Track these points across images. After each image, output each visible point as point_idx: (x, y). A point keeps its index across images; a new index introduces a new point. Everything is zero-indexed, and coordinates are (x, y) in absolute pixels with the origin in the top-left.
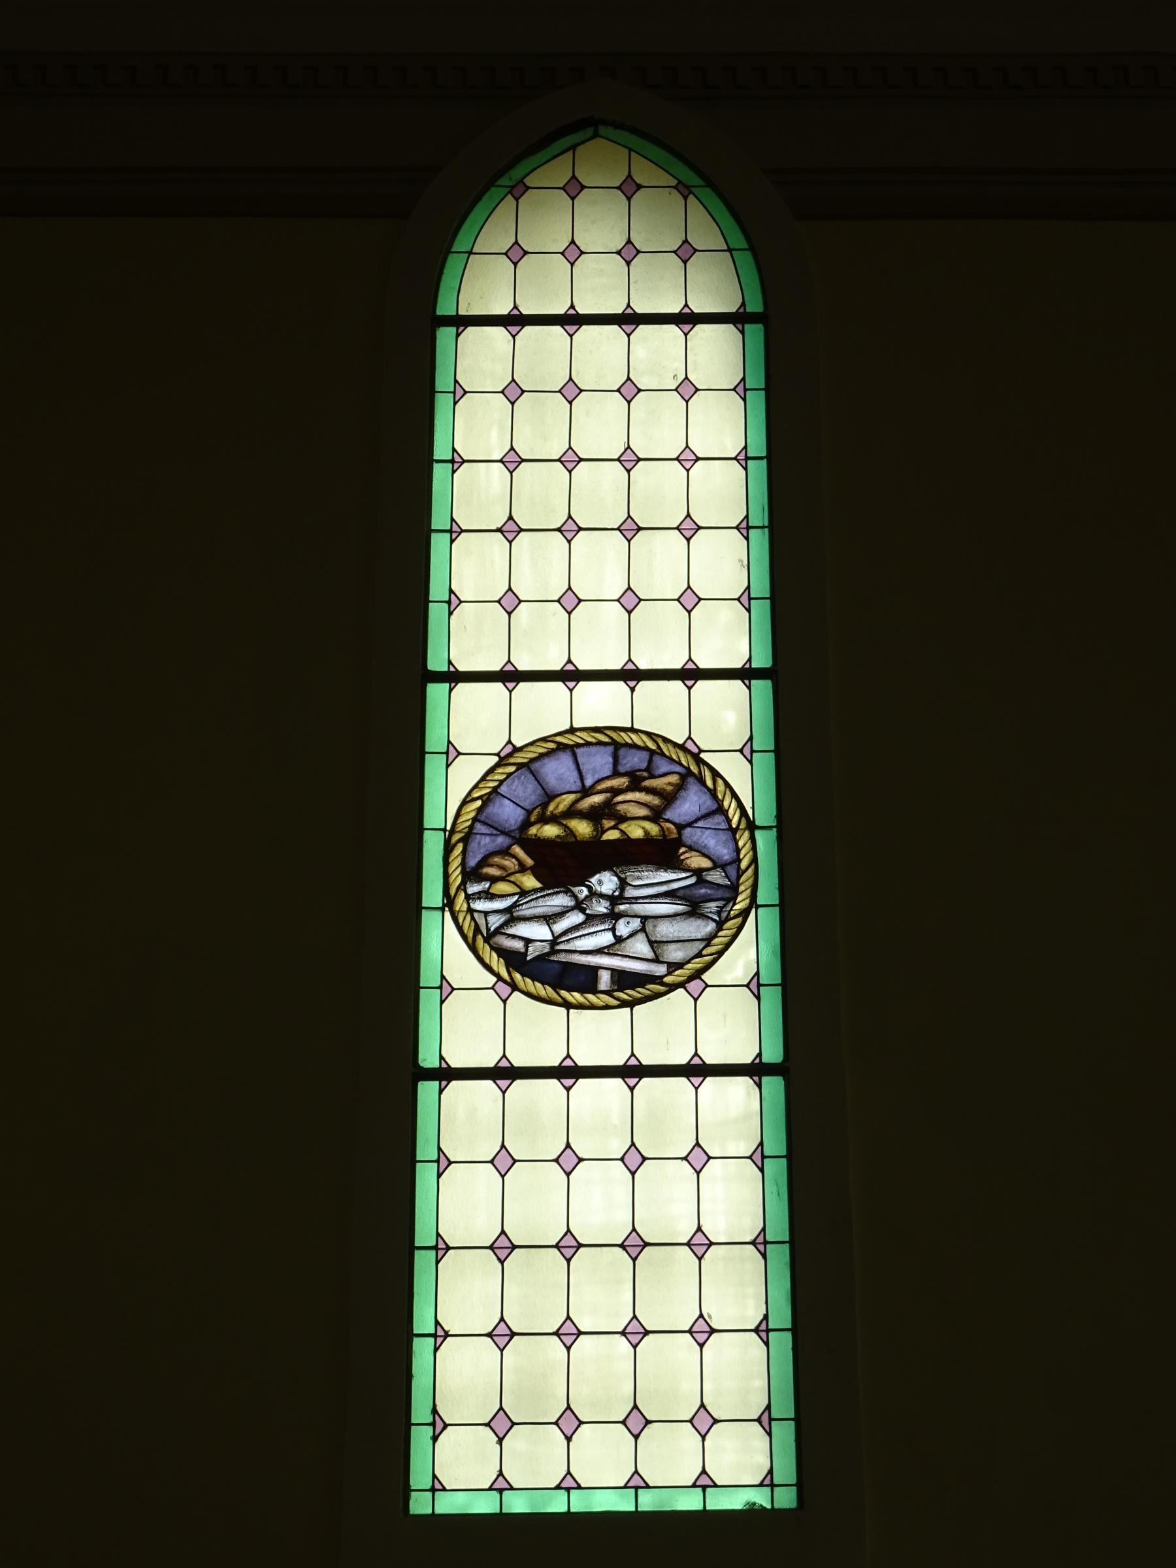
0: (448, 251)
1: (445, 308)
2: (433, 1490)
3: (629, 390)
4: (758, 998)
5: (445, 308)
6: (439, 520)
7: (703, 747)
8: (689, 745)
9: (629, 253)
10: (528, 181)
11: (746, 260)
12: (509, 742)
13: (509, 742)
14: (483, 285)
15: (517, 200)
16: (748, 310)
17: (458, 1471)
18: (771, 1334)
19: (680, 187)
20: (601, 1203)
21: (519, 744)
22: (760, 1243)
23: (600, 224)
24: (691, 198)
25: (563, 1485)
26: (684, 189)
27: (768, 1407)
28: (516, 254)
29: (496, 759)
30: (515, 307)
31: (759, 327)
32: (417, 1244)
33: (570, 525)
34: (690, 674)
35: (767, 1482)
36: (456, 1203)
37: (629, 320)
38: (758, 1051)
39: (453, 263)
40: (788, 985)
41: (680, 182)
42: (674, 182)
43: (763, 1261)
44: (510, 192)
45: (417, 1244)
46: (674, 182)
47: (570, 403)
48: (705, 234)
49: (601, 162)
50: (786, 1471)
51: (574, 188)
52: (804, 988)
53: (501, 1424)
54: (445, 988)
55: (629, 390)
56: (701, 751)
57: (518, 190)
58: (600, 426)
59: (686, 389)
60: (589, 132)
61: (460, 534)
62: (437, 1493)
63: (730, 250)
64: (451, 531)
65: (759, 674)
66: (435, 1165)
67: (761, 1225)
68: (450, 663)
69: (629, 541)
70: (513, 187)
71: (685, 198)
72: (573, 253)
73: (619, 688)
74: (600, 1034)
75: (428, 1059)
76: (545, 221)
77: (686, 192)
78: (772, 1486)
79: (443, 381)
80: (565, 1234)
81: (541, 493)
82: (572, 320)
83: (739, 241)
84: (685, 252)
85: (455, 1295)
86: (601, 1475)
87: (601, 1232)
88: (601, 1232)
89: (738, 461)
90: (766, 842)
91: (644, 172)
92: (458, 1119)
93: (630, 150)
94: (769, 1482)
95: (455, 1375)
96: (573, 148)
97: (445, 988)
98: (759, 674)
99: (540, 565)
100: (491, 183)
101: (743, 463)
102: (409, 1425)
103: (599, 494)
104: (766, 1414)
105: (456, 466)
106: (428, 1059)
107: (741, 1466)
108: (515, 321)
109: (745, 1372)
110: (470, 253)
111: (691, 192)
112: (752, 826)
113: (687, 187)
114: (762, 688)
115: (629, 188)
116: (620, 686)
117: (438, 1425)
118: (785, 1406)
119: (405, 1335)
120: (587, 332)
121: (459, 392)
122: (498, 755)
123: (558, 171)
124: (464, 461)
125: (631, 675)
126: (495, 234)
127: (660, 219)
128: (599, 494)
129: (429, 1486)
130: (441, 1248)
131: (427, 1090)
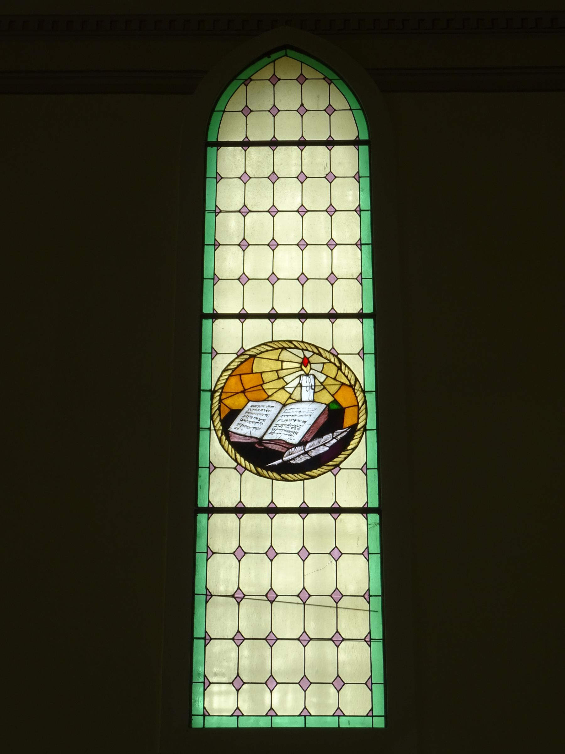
0: (213, 111)
1: (211, 138)
2: (204, 715)
3: (302, 178)
4: (366, 475)
5: (211, 138)
6: (208, 240)
7: (339, 352)
8: (333, 351)
9: (302, 110)
10: (252, 78)
11: (360, 114)
12: (242, 347)
13: (242, 347)
14: (231, 127)
15: (246, 86)
16: (361, 139)
17: (218, 704)
18: (363, 246)
19: (326, 79)
20: (287, 577)
21: (246, 349)
22: (216, 245)
23: (288, 96)
24: (332, 85)
25: (268, 714)
26: (330, 82)
27: (366, 463)
28: (247, 111)
29: (235, 356)
30: (247, 137)
31: (371, 321)
32: (196, 593)
33: (305, 637)
34: (333, 316)
35: (370, 714)
36: (218, 573)
37: (302, 143)
38: (361, 307)
39: (216, 116)
40: (381, 468)
41: (326, 77)
42: (323, 77)
43: (365, 477)
44: (243, 83)
45: (196, 593)
46: (323, 77)
47: (273, 184)
48: (339, 101)
49: (288, 67)
50: (380, 710)
51: (274, 80)
52: (390, 471)
53: (237, 683)
54: (362, 354)
55: (302, 178)
56: (338, 354)
57: (247, 82)
58: (289, 196)
59: (330, 177)
60: (282, 53)
61: (219, 213)
62: (206, 718)
63: (351, 109)
64: (215, 245)
65: (363, 143)
66: (206, 554)
67: (362, 346)
68: (214, 309)
69: (302, 251)
70: (246, 80)
71: (329, 84)
72: (274, 111)
73: (296, 322)
74: (288, 492)
75: (202, 503)
76: (260, 95)
77: (329, 82)
78: (372, 716)
79: (210, 173)
80: (270, 590)
81: (258, 227)
82: (274, 144)
83: (355, 105)
84: (330, 110)
85: (216, 620)
86: (287, 707)
87: (290, 594)
88: (290, 594)
89: (357, 245)
90: (371, 399)
91: (308, 72)
92: (219, 532)
93: (302, 62)
94: (371, 714)
95: (216, 659)
96: (274, 61)
97: (362, 354)
98: (363, 143)
99: (258, 262)
100: (235, 78)
101: (359, 246)
102: (195, 552)
103: (289, 231)
104: (360, 276)
105: (216, 247)
106: (202, 503)
107: (359, 705)
108: (246, 144)
109: (361, 659)
110: (224, 111)
111: (332, 82)
112: (364, 391)
113: (331, 80)
114: (207, 309)
115: (302, 80)
116: (296, 322)
117: (206, 683)
118: (200, 558)
119: (190, 638)
120: (280, 150)
121: (219, 178)
122: (236, 354)
123: (267, 73)
124: (221, 211)
125: (303, 316)
126: (236, 101)
127: (317, 94)
128: (289, 231)
129: (202, 713)
130: (209, 595)
131: (202, 518)
